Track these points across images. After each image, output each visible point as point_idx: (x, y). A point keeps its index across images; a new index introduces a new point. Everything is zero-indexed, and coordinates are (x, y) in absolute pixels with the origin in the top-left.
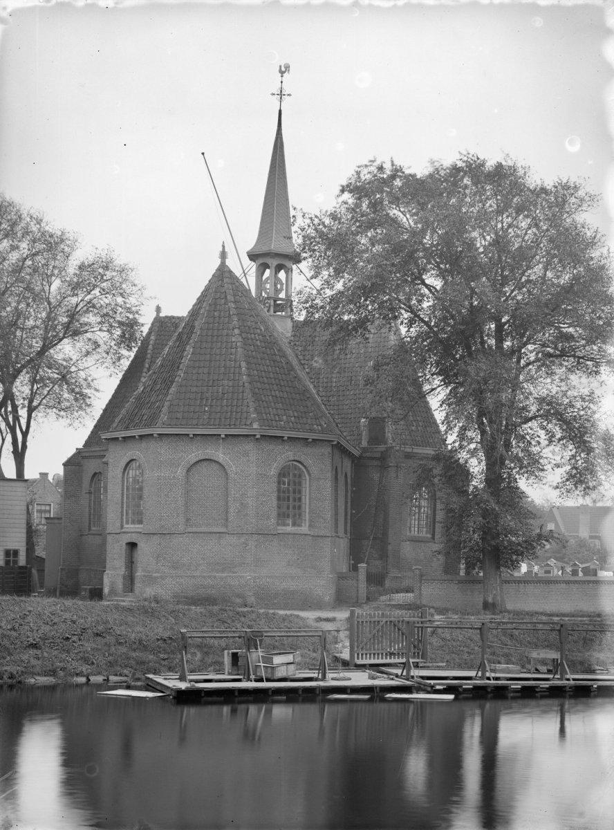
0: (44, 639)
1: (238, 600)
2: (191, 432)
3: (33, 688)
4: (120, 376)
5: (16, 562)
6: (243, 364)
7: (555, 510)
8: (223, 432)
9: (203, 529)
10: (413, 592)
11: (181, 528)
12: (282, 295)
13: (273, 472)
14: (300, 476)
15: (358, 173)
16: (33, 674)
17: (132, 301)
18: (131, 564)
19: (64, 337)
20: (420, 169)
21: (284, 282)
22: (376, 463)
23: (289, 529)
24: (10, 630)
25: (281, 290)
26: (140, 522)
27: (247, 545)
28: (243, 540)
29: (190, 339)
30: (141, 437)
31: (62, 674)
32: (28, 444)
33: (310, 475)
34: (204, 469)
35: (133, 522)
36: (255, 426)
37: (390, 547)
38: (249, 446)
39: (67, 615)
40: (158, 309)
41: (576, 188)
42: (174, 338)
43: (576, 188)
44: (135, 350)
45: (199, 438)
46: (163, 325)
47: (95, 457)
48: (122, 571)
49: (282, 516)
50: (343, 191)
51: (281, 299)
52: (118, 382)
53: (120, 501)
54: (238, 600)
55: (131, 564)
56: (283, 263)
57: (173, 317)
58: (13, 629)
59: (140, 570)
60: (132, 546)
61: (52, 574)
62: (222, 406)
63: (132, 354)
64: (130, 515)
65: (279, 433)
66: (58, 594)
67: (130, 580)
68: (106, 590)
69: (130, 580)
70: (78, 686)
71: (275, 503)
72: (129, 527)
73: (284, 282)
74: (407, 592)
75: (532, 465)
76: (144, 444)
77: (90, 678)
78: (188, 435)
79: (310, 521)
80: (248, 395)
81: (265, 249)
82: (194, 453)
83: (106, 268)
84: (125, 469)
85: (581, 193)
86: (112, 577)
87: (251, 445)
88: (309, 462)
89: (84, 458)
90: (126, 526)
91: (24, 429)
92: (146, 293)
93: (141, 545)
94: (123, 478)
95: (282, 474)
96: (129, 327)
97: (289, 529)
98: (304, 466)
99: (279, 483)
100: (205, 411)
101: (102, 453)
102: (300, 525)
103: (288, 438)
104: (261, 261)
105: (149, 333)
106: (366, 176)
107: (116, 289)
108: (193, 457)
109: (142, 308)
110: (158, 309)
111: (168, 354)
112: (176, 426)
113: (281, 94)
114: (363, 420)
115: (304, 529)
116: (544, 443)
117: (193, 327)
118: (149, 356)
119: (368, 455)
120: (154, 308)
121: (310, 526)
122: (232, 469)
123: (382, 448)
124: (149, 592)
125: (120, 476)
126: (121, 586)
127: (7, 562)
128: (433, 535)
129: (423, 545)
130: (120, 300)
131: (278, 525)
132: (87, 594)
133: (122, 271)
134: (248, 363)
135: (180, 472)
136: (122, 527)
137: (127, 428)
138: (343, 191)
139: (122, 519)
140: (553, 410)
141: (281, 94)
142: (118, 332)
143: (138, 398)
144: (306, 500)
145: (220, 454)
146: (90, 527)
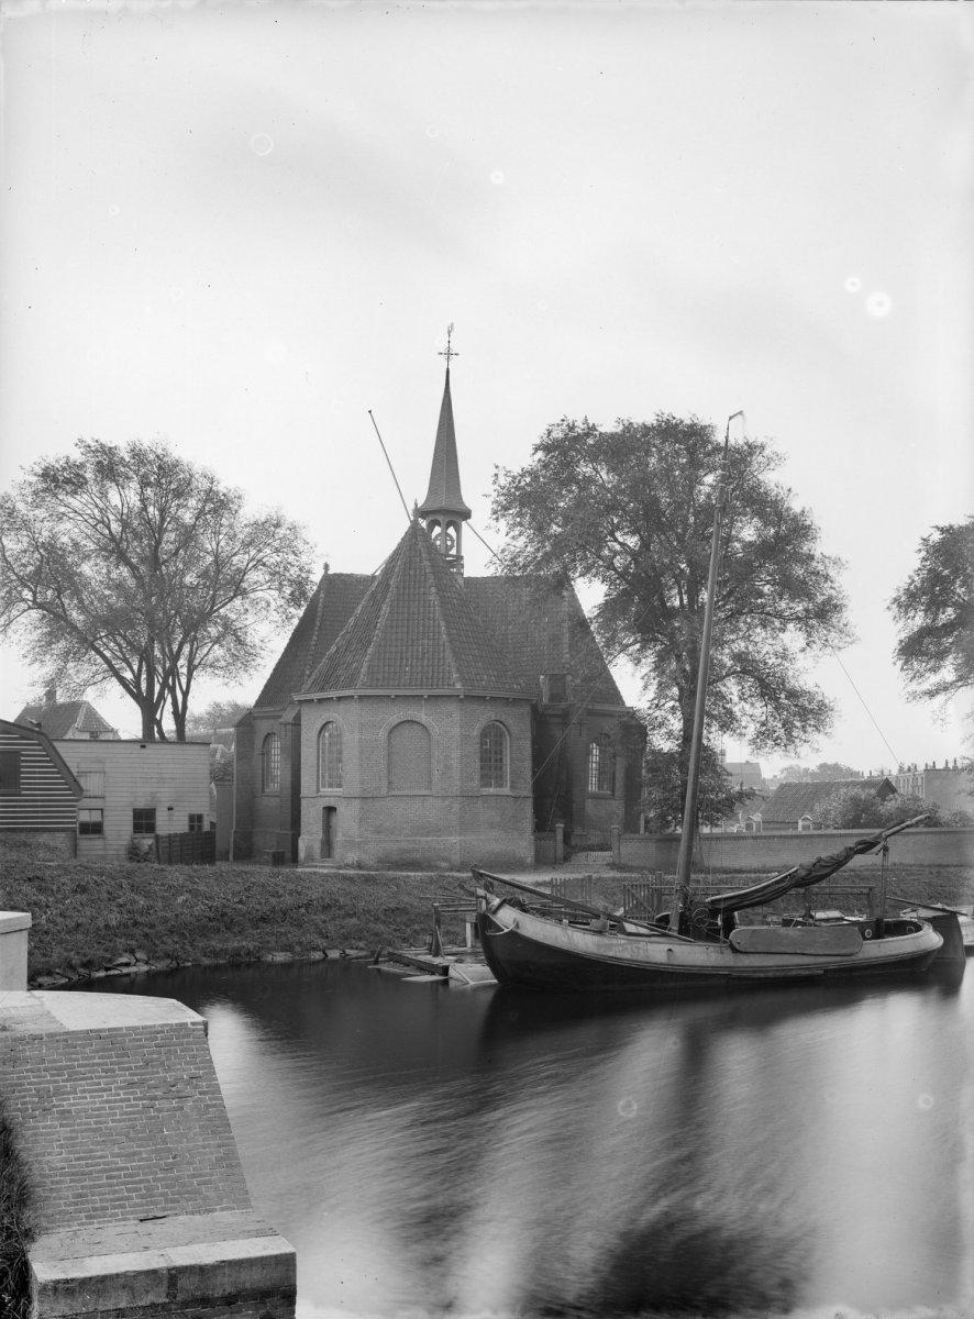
0: (273, 910)
1: (444, 864)
2: (393, 693)
3: (271, 965)
4: (289, 635)
5: (200, 827)
6: (442, 623)
7: (82, 712)
8: (426, 693)
9: (405, 792)
10: (610, 849)
11: (384, 791)
12: (453, 552)
13: (476, 733)
14: (501, 735)
15: (549, 433)
16: (270, 950)
17: (304, 559)
18: (328, 829)
19: (235, 596)
20: (608, 426)
21: (455, 537)
22: (556, 720)
23: (492, 790)
24: (239, 903)
25: (452, 547)
26: (340, 786)
27: (452, 808)
28: (447, 803)
29: (385, 598)
30: (339, 699)
31: (298, 949)
32: (189, 704)
33: (511, 735)
34: (406, 731)
35: (331, 786)
36: (458, 686)
37: (574, 805)
38: (453, 707)
39: (291, 886)
40: (326, 567)
41: (763, 447)
42: (366, 597)
43: (763, 447)
44: (303, 609)
45: (400, 699)
46: (337, 585)
47: (268, 718)
48: (320, 836)
49: (485, 780)
50: (536, 450)
51: (451, 556)
52: (287, 641)
53: (315, 762)
54: (444, 864)
55: (328, 829)
56: (454, 519)
57: (342, 575)
58: (240, 902)
59: (340, 834)
60: (330, 810)
61: (226, 839)
62: (423, 666)
63: (301, 612)
64: (327, 779)
65: (419, 692)
66: (231, 858)
67: (327, 846)
68: (302, 855)
69: (327, 846)
70: (318, 962)
71: (478, 764)
72: (326, 790)
73: (455, 537)
74: (602, 850)
75: (728, 722)
76: (342, 706)
77: (328, 952)
78: (389, 696)
79: (512, 782)
80: (448, 653)
81: (436, 506)
82: (396, 714)
83: (277, 526)
84: (320, 732)
85: (767, 452)
86: (310, 839)
87: (454, 705)
88: (510, 722)
89: (255, 718)
90: (322, 790)
91: (184, 687)
92: (318, 551)
93: (341, 809)
94: (318, 742)
95: (484, 734)
96: (300, 585)
97: (492, 790)
98: (508, 731)
99: (482, 745)
100: (405, 672)
101: (277, 714)
102: (501, 786)
103: (491, 697)
104: (431, 518)
105: (318, 591)
106: (558, 434)
107: (288, 546)
108: (394, 719)
109: (313, 565)
110: (326, 567)
111: (362, 613)
112: (377, 687)
113: (449, 354)
114: (542, 677)
115: (506, 790)
116: (735, 699)
117: (388, 585)
118: (320, 614)
119: (550, 712)
120: (322, 566)
121: (511, 786)
122: (435, 730)
123: (563, 705)
124: (352, 857)
125: (315, 738)
126: (318, 851)
127: (192, 828)
128: (613, 791)
129: (603, 802)
130: (291, 558)
131: (481, 787)
132: (270, 858)
133: (293, 528)
134: (447, 622)
135: (382, 734)
136: (318, 791)
137: (322, 689)
138: (536, 450)
139: (318, 783)
140: (747, 666)
141: (449, 354)
142: (288, 591)
143: (331, 659)
144: (507, 760)
145: (422, 714)
146: (263, 788)
